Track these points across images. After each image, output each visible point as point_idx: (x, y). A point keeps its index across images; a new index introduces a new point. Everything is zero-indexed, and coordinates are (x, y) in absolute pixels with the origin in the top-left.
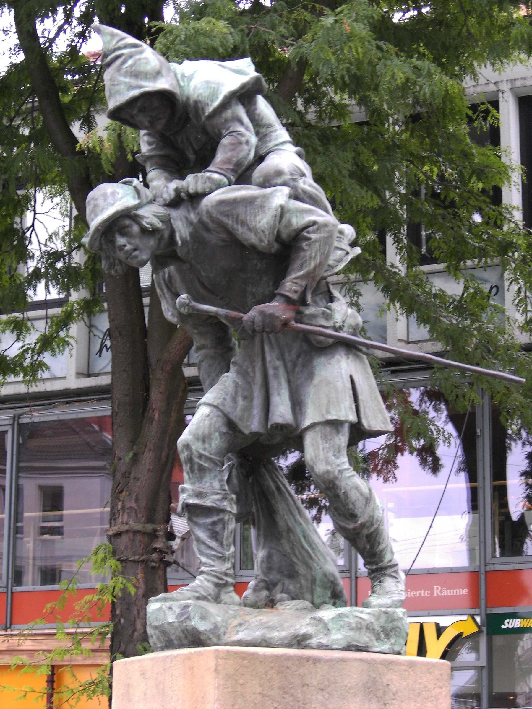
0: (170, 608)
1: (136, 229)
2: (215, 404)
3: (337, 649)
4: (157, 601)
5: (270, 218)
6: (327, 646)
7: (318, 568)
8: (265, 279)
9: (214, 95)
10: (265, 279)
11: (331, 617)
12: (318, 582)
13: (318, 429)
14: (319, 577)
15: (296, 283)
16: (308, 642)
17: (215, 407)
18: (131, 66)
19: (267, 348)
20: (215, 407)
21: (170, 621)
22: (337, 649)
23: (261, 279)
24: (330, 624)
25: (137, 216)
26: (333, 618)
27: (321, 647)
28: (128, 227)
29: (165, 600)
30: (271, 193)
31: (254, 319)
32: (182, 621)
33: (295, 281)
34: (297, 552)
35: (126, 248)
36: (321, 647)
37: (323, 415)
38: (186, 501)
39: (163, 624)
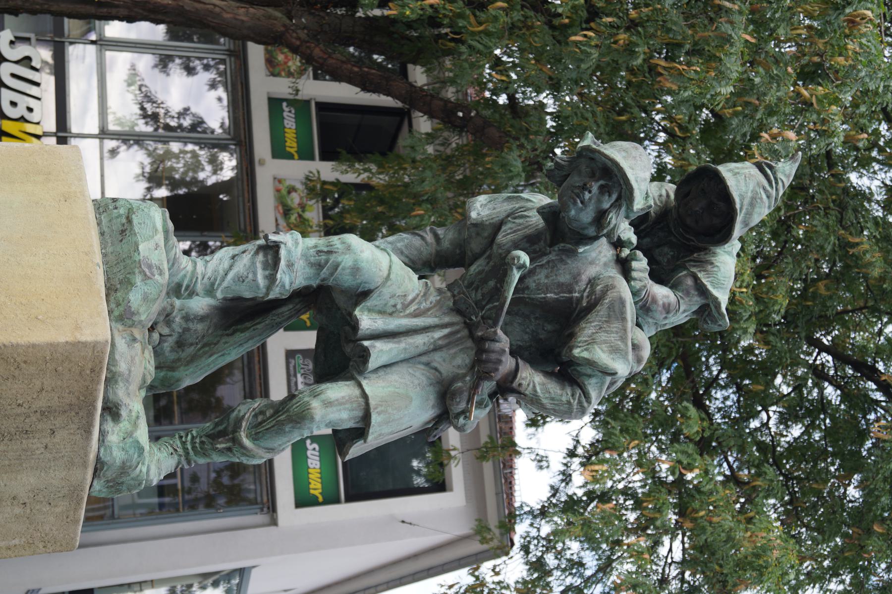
0: (157, 246)
1: (606, 205)
2: (391, 276)
3: (42, 109)
4: (164, 221)
5: (605, 362)
6: (103, 441)
7: (187, 372)
8: (526, 337)
9: (709, 274)
10: (526, 337)
11: (140, 440)
12: (170, 374)
13: (361, 400)
14: (176, 374)
15: (528, 385)
16: (109, 418)
17: (388, 277)
18: (761, 199)
19: (446, 331)
20: (388, 277)
21: (141, 247)
22: (42, 109)
23: (527, 333)
24: (131, 440)
25: (620, 207)
26: (138, 442)
27: (103, 434)
28: (610, 196)
29: (166, 232)
30: (627, 360)
31: (497, 341)
32: (140, 266)
33: (531, 385)
34: (207, 349)
35: (587, 193)
36: (103, 434)
37: (376, 408)
38: (282, 246)
39: (135, 234)
